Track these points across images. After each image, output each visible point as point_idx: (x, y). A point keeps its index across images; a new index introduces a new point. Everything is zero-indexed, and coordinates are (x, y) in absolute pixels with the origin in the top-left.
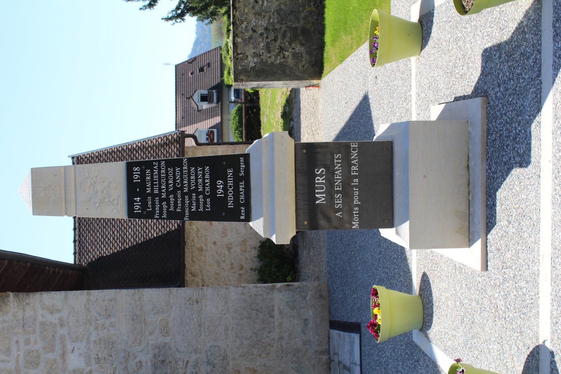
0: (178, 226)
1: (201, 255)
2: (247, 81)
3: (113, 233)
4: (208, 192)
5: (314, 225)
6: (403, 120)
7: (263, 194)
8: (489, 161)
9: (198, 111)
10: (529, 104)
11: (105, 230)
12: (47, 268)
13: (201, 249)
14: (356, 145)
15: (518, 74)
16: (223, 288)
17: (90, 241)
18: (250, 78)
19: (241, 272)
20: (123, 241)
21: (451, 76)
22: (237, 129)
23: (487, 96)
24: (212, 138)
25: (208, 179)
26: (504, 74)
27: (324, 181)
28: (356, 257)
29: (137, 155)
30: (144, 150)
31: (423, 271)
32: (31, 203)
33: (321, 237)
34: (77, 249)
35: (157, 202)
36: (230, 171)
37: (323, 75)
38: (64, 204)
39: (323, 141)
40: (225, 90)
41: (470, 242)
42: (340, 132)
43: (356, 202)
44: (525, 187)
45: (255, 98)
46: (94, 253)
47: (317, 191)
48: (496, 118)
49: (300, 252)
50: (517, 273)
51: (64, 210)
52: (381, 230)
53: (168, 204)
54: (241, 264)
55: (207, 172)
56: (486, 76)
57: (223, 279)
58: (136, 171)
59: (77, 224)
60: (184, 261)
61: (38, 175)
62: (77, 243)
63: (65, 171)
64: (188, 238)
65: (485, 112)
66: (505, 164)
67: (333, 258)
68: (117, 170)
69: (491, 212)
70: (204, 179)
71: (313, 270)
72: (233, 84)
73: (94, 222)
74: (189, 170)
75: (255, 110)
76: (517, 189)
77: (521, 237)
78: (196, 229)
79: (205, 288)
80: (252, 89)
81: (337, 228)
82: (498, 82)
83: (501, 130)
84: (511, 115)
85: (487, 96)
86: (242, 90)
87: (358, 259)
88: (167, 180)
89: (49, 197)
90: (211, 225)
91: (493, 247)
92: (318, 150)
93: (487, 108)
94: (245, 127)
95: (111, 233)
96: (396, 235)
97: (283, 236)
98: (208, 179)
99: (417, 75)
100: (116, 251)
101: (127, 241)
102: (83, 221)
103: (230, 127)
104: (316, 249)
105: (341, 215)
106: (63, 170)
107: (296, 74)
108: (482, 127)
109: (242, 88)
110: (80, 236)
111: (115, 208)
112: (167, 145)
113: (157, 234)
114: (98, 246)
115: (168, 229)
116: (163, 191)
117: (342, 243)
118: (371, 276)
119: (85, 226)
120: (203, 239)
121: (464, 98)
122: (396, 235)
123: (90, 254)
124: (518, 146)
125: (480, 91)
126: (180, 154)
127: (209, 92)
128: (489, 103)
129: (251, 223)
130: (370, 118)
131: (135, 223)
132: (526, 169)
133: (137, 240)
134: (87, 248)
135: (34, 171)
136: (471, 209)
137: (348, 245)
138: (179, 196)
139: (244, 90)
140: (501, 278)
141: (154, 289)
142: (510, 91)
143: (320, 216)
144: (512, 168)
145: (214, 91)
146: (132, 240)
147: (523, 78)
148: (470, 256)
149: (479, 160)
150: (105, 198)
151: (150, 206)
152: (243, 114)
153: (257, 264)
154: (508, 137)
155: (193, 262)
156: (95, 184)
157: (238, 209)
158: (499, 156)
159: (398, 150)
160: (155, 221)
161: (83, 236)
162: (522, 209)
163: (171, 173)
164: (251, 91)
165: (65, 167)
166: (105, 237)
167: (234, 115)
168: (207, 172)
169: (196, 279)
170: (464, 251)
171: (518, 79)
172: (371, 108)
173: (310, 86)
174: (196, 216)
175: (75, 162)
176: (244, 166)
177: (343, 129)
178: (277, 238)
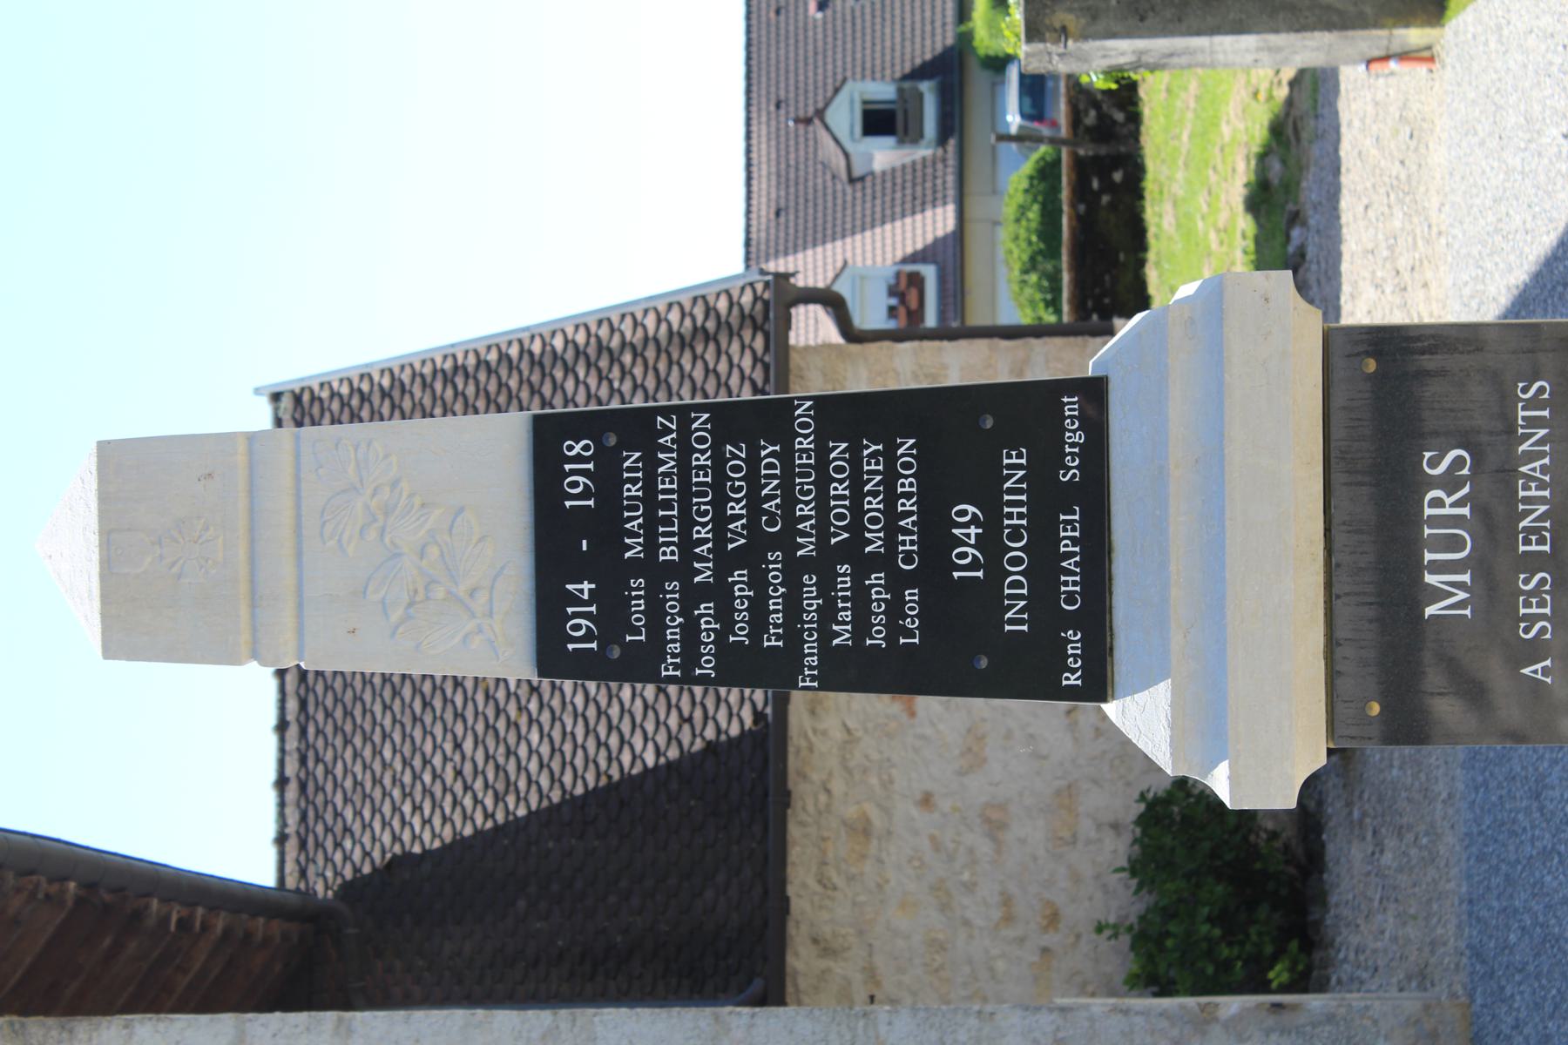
0: (758, 716)
1: (863, 857)
2: (1085, 37)
3: (458, 746)
4: (908, 559)
5: (1407, 725)
9: (852, 180)
11: (418, 734)
12: (155, 904)
13: (862, 830)
16: (966, 1013)
17: (348, 784)
18: (1098, 23)
19: (1051, 939)
20: (500, 786)
22: (1031, 265)
24: (914, 305)
25: (908, 496)
27: (1466, 511)
29: (570, 385)
30: (604, 363)
32: (97, 604)
33: (1437, 779)
34: (293, 817)
35: (672, 605)
36: (1015, 460)
37: (1449, 13)
38: (244, 611)
39: (1450, 317)
40: (978, 80)
42: (1537, 277)
45: (1119, 116)
46: (367, 840)
47: (1428, 556)
51: (245, 636)
53: (725, 615)
54: (1049, 903)
55: (907, 466)
57: (967, 969)
58: (579, 459)
59: (292, 705)
60: (782, 882)
61: (128, 471)
62: (292, 792)
63: (250, 452)
64: (804, 776)
67: (1496, 881)
68: (499, 444)
70: (891, 498)
71: (1394, 939)
72: (1022, 50)
73: (367, 697)
74: (822, 452)
75: (1118, 176)
78: (838, 735)
79: (882, 1011)
80: (1108, 73)
81: (1518, 737)
86: (1055, 77)
88: (720, 502)
89: (179, 576)
90: (912, 714)
92: (1429, 362)
95: (448, 747)
97: (1259, 775)
98: (908, 496)
100: (468, 831)
101: (522, 784)
102: (320, 688)
103: (1001, 254)
104: (1410, 837)
106: (242, 447)
109: (1063, 68)
110: (303, 760)
111: (480, 631)
112: (708, 337)
113: (658, 753)
114: (387, 809)
115: (710, 733)
116: (701, 550)
117: (1541, 809)
119: (328, 715)
120: (874, 781)
123: (348, 844)
126: (766, 380)
127: (900, 91)
129: (1110, 708)
131: (556, 703)
133: (568, 778)
134: (337, 814)
135: (107, 451)
138: (775, 575)
139: (1073, 82)
141: (645, 1013)
143: (1434, 678)
145: (927, 88)
146: (544, 781)
150: (431, 583)
151: (638, 619)
153: (1124, 901)
155: (824, 885)
156: (386, 514)
157: (1055, 645)
160: (650, 690)
161: (318, 760)
163: (736, 469)
164: (1099, 82)
165: (251, 438)
166: (417, 763)
167: (1020, 198)
168: (907, 466)
169: (838, 968)
173: (1386, 58)
174: (852, 671)
175: (286, 417)
176: (1079, 438)
178: (1234, 779)
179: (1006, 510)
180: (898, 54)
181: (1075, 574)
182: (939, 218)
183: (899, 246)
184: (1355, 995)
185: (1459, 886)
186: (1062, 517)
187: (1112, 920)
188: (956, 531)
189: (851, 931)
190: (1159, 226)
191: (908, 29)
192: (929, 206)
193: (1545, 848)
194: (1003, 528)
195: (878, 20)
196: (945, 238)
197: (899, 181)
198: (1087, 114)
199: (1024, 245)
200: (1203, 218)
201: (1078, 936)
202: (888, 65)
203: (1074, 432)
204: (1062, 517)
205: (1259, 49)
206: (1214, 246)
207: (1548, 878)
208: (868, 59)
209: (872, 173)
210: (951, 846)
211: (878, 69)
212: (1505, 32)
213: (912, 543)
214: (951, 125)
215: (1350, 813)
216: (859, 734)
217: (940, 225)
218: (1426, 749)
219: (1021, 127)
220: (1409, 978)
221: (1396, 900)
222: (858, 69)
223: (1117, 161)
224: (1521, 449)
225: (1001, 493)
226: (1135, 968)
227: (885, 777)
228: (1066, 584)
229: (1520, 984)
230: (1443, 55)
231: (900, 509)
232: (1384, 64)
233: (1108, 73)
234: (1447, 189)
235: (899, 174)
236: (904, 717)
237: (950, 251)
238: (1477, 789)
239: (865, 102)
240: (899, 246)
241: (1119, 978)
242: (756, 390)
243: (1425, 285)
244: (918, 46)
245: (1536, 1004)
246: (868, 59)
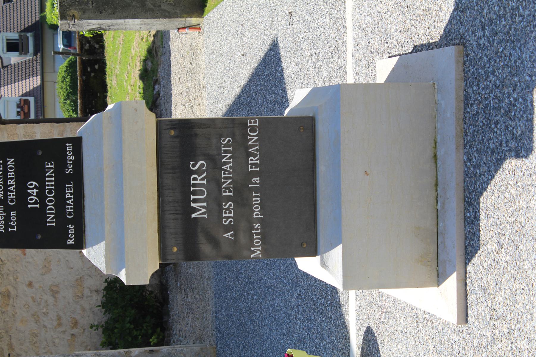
2: (81, 19)
5: (192, 253)
6: (334, 82)
7: (105, 203)
8: (468, 147)
10: (530, 57)
14: (255, 122)
15: (513, 9)
18: (85, 15)
19: (75, 331)
21: (408, 12)
22: (67, 97)
23: (464, 45)
24: (26, 111)
25: (12, 179)
26: (491, 9)
27: (205, 182)
28: (261, 304)
31: (366, 325)
33: (204, 272)
36: (50, 166)
37: (206, 10)
40: (48, 33)
41: (439, 278)
42: (235, 102)
43: (257, 214)
44: (525, 189)
45: (97, 46)
48: (478, 79)
49: (170, 296)
50: (513, 327)
52: (297, 259)
56: (462, 12)
65: (461, 69)
66: (493, 152)
69: (473, 228)
72: (59, 23)
75: (97, 67)
76: (513, 192)
77: (519, 268)
80: (90, 31)
81: (230, 257)
82: (480, 21)
83: (486, 99)
84: (502, 74)
85: (464, 45)
87: (263, 306)
90: (25, 254)
91: (476, 285)
93: (464, 63)
94: (81, 94)
96: (322, 268)
97: (138, 270)
98: (12, 179)
99: (354, 11)
103: (57, 93)
105: (232, 235)
107: (163, 7)
108: (457, 94)
109: (73, 29)
118: (284, 335)
120: (11, 278)
121: (429, 46)
122: (322, 268)
124: (513, 124)
125: (453, 36)
127: (20, 36)
128: (467, 55)
129: (84, 251)
130: (281, 79)
132: (526, 161)
136: (441, 225)
137: (248, 284)
140: (489, 334)
142: (500, 36)
143: (202, 239)
144: (505, 159)
145: (29, 35)
147: (520, 15)
148: (439, 300)
149: (453, 147)
152: (78, 73)
153: (100, 317)
154: (498, 109)
157: (64, 230)
158: (483, 140)
159: (321, 129)
162: (520, 223)
164: (87, 35)
167: (63, 74)
170: (432, 291)
171: (513, 16)
172: (283, 64)
173: (185, 28)
176: (72, 158)
177: (239, 97)
178: (127, 275)
179: (47, 183)
180: (19, 23)
181: (71, 205)
182: (35, 81)
183: (21, 90)
184: (179, 346)
185: (212, 307)
186: (67, 186)
187: (96, 324)
188: (29, 191)
189: (3, 331)
190: (111, 84)
191: (22, 14)
192: (31, 76)
193: (240, 294)
194: (46, 189)
195: (12, 11)
196: (37, 87)
197: (20, 67)
198: (85, 46)
199: (65, 90)
200: (126, 81)
201: (84, 330)
202: (16, 27)
203: (71, 156)
204: (67, 186)
205: (141, 24)
206: (130, 91)
207: (241, 304)
208: (8, 24)
209: (11, 65)
210: (39, 300)
211: (12, 28)
212: (223, 20)
213: (13, 195)
214: (39, 48)
215: (177, 284)
216: (6, 262)
217: (35, 83)
218: (201, 262)
219: (63, 49)
220: (197, 339)
221: (192, 313)
222: (5, 28)
223: (97, 62)
224: (223, 161)
225: (45, 177)
226: (104, 340)
227: (15, 277)
228: (68, 209)
229: (232, 340)
230: (203, 27)
231: (9, 183)
232: (184, 30)
233: (90, 31)
234: (205, 72)
235: (20, 65)
236: (22, 255)
237: (39, 92)
238: (218, 274)
239: (7, 40)
240: (21, 90)
241: (99, 344)
243: (199, 105)
244: (26, 20)
245: (237, 346)
246: (8, 24)
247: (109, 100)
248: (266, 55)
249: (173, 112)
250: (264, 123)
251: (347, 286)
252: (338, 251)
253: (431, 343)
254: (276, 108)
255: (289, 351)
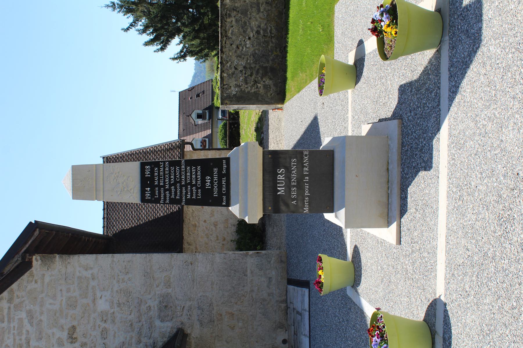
0: (179, 208)
2: (230, 105)
3: (132, 213)
5: (277, 210)
6: (342, 135)
13: (195, 226)
15: (424, 104)
23: (402, 119)
26: (414, 103)
33: (282, 218)
34: (106, 224)
35: (162, 192)
36: (216, 170)
38: (95, 192)
39: (285, 149)
40: (215, 110)
41: (388, 224)
43: (307, 193)
44: (428, 185)
48: (408, 135)
51: (95, 196)
52: (324, 214)
53: (170, 193)
58: (148, 169)
59: (106, 206)
61: (76, 170)
66: (414, 168)
68: (135, 167)
70: (196, 175)
72: (220, 106)
74: (186, 168)
81: (294, 212)
83: (411, 144)
84: (419, 133)
85: (402, 119)
88: (170, 176)
97: (253, 217)
99: (352, 103)
106: (95, 167)
107: (266, 100)
110: (107, 215)
115: (171, 211)
121: (386, 119)
124: (423, 155)
125: (397, 115)
128: (403, 124)
129: (230, 208)
130: (319, 133)
132: (429, 172)
136: (390, 200)
138: (178, 187)
140: (410, 250)
142: (418, 116)
143: (281, 204)
145: (207, 111)
147: (427, 107)
148: (388, 234)
153: (235, 237)
157: (220, 197)
159: (337, 156)
164: (232, 112)
169: (191, 247)
171: (424, 107)
174: (191, 202)
176: (225, 166)
177: (299, 140)
178: (248, 219)
214: (211, 117)
242: (179, 158)
247: (241, 141)
248: (312, 122)
249: (270, 146)
250: (312, 153)
251: (346, 227)
252: (343, 211)
253: (384, 253)
254: (316, 146)
255: (320, 255)
